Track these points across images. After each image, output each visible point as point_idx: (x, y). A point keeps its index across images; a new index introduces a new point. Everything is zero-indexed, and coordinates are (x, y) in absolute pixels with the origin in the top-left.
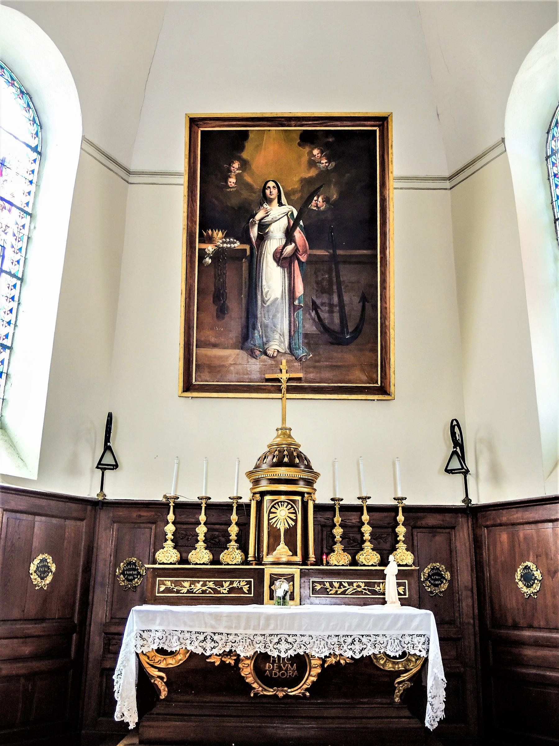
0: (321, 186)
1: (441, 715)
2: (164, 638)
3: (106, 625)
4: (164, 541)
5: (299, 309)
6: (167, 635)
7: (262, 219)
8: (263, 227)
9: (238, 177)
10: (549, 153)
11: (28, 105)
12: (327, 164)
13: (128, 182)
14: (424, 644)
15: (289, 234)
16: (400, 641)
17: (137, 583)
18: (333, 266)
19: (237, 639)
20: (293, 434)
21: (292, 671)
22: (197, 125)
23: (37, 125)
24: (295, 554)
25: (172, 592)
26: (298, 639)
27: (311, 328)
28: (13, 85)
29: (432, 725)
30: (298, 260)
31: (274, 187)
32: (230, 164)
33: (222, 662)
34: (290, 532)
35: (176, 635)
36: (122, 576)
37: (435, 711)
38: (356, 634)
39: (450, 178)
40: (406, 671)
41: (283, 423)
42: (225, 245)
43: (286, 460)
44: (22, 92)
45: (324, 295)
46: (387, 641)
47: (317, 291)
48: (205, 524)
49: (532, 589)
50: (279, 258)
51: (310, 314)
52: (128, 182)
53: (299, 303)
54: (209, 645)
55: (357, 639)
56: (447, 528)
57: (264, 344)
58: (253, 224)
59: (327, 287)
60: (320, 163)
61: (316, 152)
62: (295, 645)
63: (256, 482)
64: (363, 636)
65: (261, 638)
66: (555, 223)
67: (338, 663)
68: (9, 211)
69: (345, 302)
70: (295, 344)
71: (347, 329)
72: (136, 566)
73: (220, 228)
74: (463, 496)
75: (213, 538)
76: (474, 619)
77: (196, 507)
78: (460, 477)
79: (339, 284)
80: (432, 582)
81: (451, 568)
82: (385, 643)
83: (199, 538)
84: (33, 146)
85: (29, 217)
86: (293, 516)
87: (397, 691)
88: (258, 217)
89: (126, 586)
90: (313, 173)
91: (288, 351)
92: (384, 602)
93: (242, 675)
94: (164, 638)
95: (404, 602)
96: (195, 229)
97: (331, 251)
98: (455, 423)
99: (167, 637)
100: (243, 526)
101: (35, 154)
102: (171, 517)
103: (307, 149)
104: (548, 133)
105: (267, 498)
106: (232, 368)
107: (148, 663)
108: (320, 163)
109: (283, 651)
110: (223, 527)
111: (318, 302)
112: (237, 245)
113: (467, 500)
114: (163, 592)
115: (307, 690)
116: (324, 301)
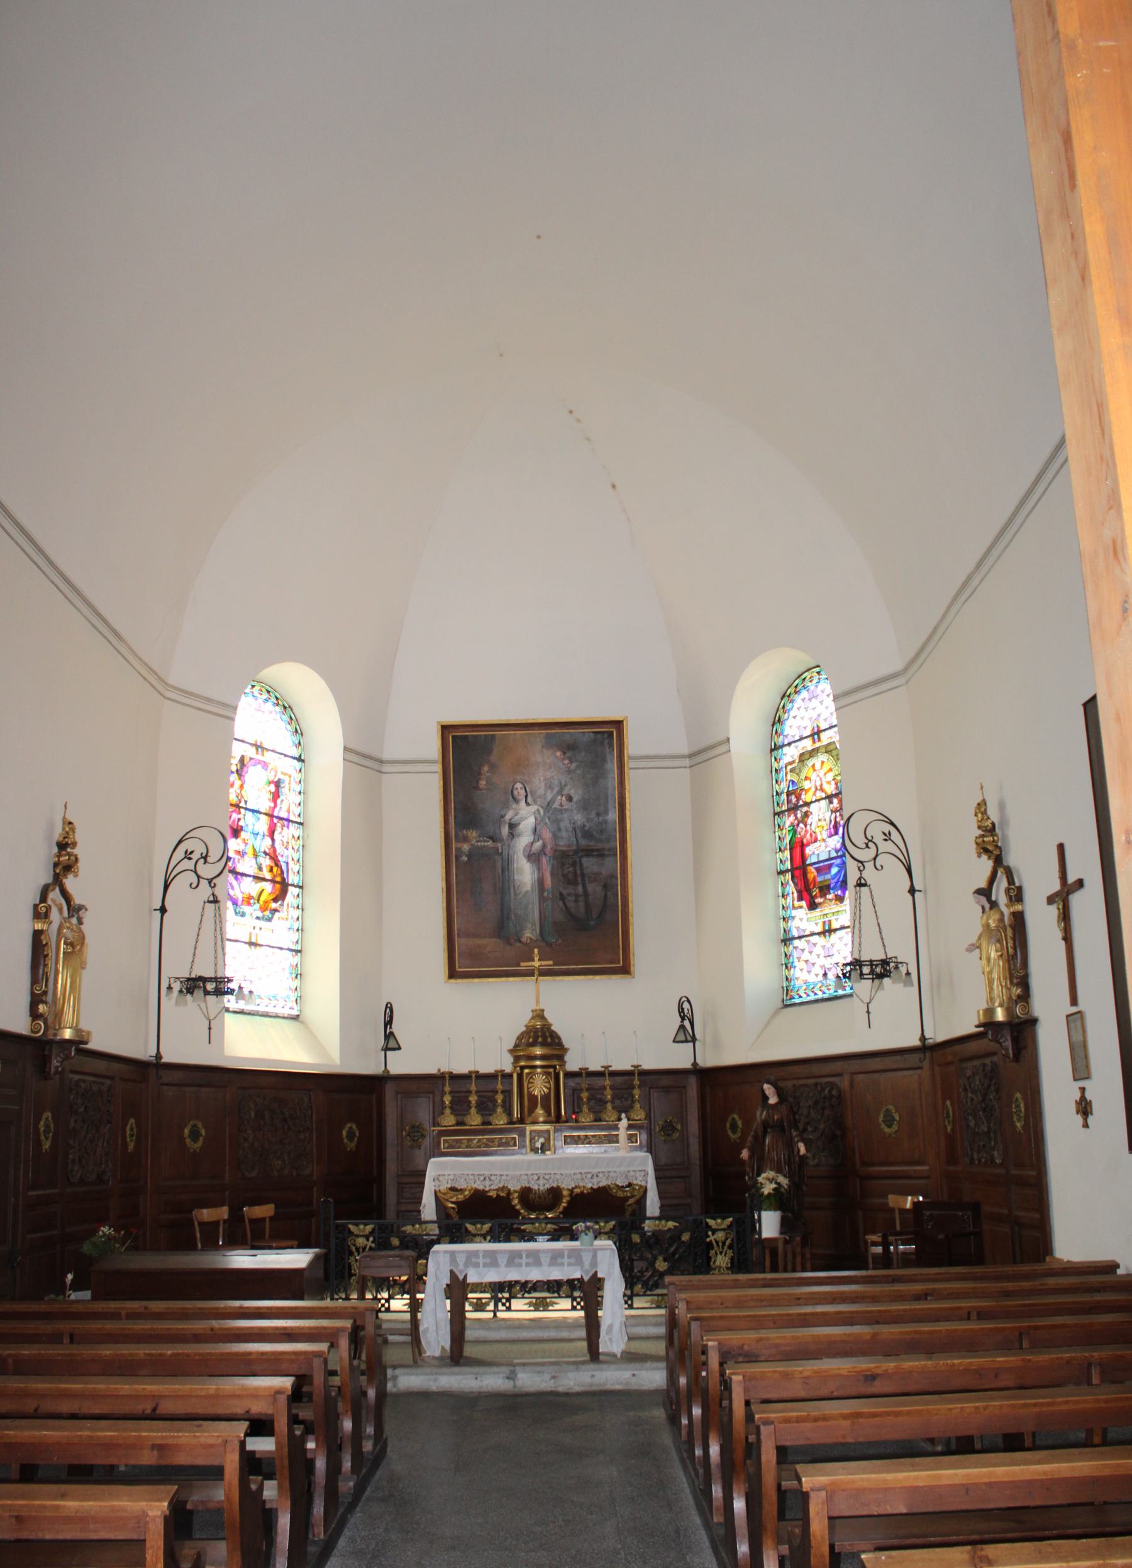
8: (512, 826)
20: (546, 1014)
24: (549, 1114)
27: (560, 917)
28: (277, 704)
33: (498, 1195)
34: (546, 1098)
38: (595, 1171)
39: (690, 756)
40: (632, 1196)
43: (540, 1040)
44: (285, 708)
54: (487, 1183)
63: (517, 1059)
67: (582, 1192)
77: (466, 1077)
84: (297, 756)
88: (508, 817)
100: (508, 1093)
102: (447, 1089)
105: (526, 1071)
110: (490, 1094)
111: (565, 892)
113: (695, 1064)
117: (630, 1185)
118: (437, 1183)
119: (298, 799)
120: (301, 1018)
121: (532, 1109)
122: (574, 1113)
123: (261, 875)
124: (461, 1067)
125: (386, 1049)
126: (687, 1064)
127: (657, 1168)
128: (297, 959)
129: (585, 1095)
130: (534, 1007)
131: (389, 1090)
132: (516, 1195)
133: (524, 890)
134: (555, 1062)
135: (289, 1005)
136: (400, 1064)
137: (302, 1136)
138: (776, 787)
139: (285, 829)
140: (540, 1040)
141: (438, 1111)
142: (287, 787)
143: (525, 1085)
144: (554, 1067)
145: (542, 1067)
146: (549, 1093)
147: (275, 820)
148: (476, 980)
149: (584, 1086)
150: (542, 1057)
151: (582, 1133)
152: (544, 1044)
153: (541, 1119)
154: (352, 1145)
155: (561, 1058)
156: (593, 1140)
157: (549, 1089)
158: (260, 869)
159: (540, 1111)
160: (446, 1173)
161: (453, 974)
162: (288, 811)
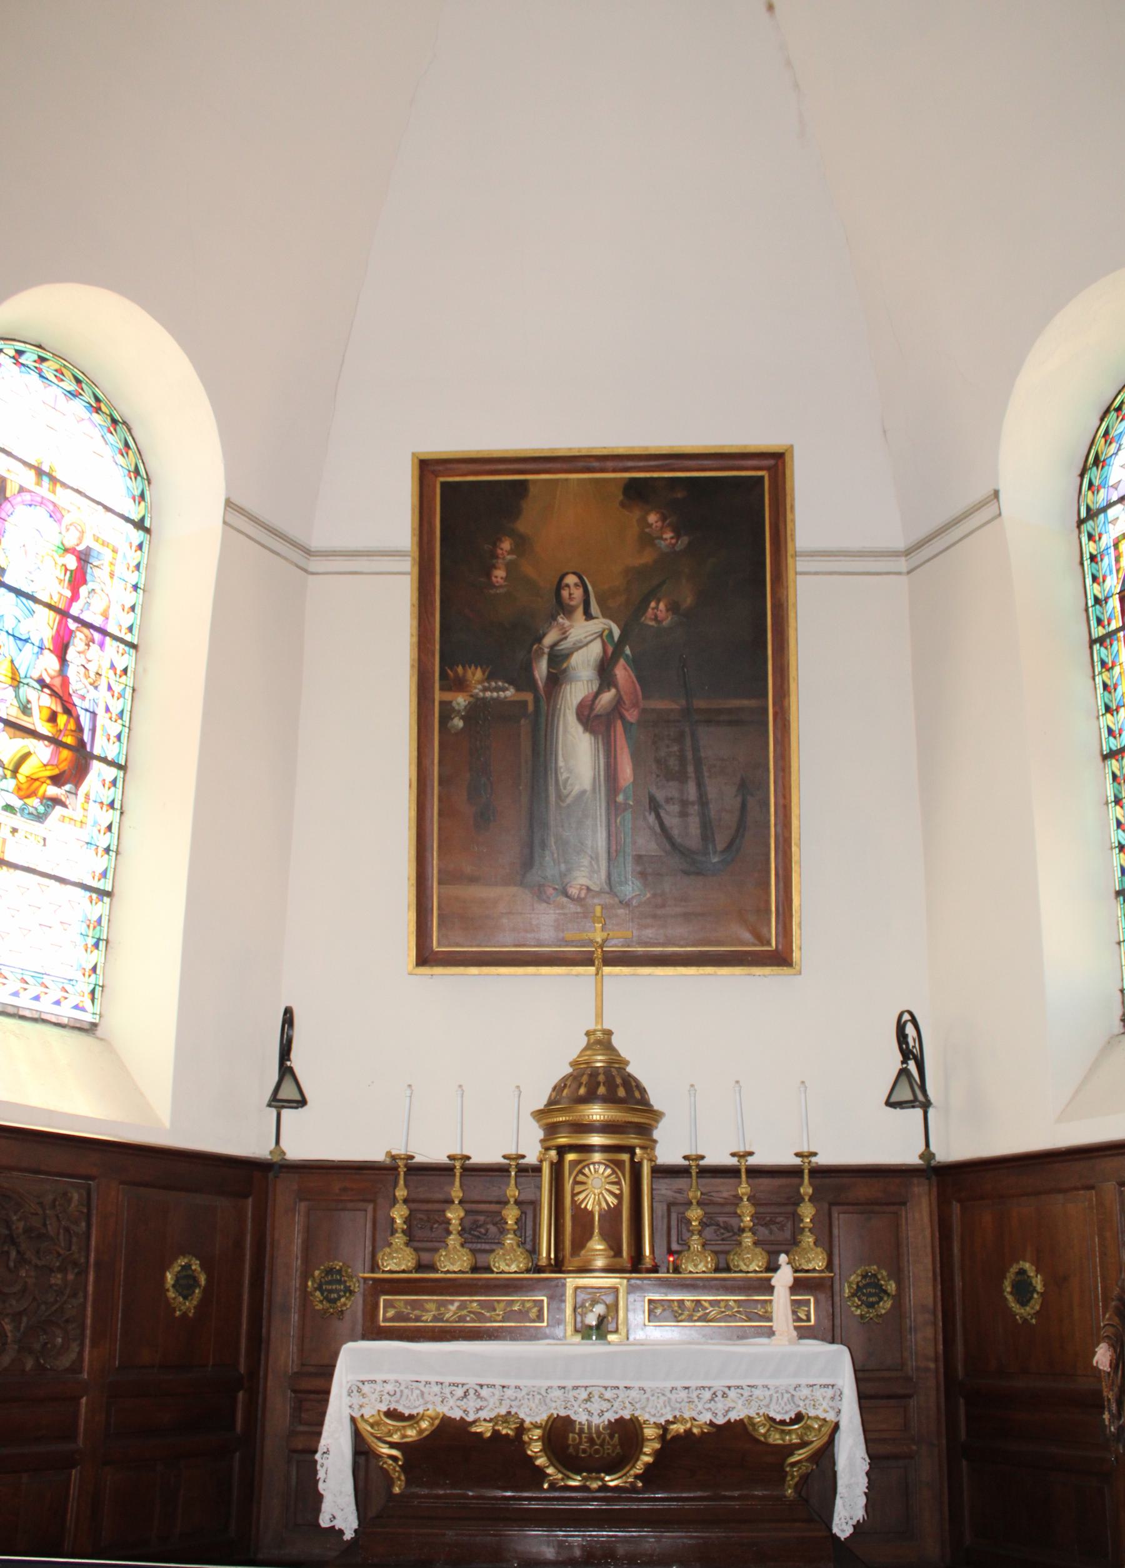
0: (664, 582)
1: (859, 1514)
2: (398, 1394)
3: (297, 1375)
4: (389, 1233)
5: (625, 810)
6: (402, 1388)
7: (556, 644)
8: (558, 659)
9: (510, 567)
10: (1083, 514)
11: (127, 445)
12: (673, 541)
13: (306, 571)
14: (833, 1398)
15: (605, 671)
16: (793, 1396)
17: (345, 1304)
18: (687, 729)
19: (520, 1395)
20: (616, 1041)
21: (612, 1448)
22: (433, 472)
23: (142, 478)
24: (618, 1253)
25: (406, 1319)
26: (622, 1394)
27: (648, 844)
28: (98, 410)
29: (843, 1531)
30: (622, 717)
31: (576, 585)
32: (495, 544)
33: (496, 1433)
34: (612, 1216)
35: (417, 1388)
36: (318, 1293)
37: (849, 1510)
38: (719, 1384)
39: (908, 553)
40: (804, 1444)
41: (597, 1023)
42: (488, 694)
43: (602, 1090)
44: (114, 422)
45: (671, 783)
46: (771, 1396)
47: (658, 776)
48: (461, 1202)
49: (1028, 1308)
50: (587, 716)
51: (645, 818)
52: (306, 571)
53: (626, 799)
55: (719, 1394)
56: (894, 1204)
57: (563, 875)
58: (540, 653)
59: (677, 768)
60: (661, 538)
61: (652, 518)
62: (616, 1404)
63: (551, 1130)
64: (729, 1388)
65: (559, 1393)
66: (1091, 648)
67: (688, 1432)
68: (102, 645)
69: (710, 797)
70: (619, 875)
71: (714, 846)
72: (342, 1276)
73: (477, 662)
74: (922, 1148)
75: (476, 1225)
76: (936, 1360)
77: (442, 1171)
78: (919, 1112)
79: (698, 762)
80: (864, 1298)
81: (898, 1274)
82: (768, 1399)
83: (451, 1228)
85: (132, 651)
86: (615, 1189)
87: (789, 1478)
88: (548, 640)
89: (325, 1311)
90: (647, 557)
91: (607, 888)
92: (770, 1333)
93: (529, 1452)
94: (398, 1394)
95: (804, 1333)
96: (433, 665)
97: (683, 702)
98: (906, 1017)
99: (402, 1391)
101: (141, 533)
102: (401, 1193)
103: (637, 514)
104: (1082, 476)
105: (571, 1157)
106: (504, 921)
107: (372, 1434)
108: (661, 538)
109: (596, 1414)
110: (494, 1207)
111: (660, 796)
112: (510, 693)
113: (927, 1155)
114: (392, 1320)
115: (637, 1477)
116: (670, 795)
117: (799, 1418)
118: (357, 1400)
119: (132, 598)
120: (100, 1032)
121: (580, 1243)
122: (671, 1252)
123: (25, 721)
124: (432, 1150)
125: (277, 1102)
126: (909, 1155)
127: (861, 1375)
128: (101, 908)
129: (695, 1214)
130: (592, 1026)
131: (283, 1193)
132: (537, 1433)
133: (576, 789)
134: (632, 1140)
135: (74, 1000)
136: (308, 1139)
137: (57, 1279)
138: (1095, 590)
139: (95, 647)
140: (602, 1090)
141: (381, 1231)
142: (107, 569)
143: (568, 1186)
144: (631, 1150)
145: (605, 1149)
146: (618, 1209)
147: (72, 625)
148: (474, 970)
149: (694, 1194)
150: (607, 1128)
151: (688, 1297)
152: (610, 1099)
153: (600, 1263)
154: (187, 1306)
155: (644, 1131)
156: (713, 1312)
157: (619, 1197)
158: (25, 709)
159: (597, 1245)
160: (379, 1377)
161: (425, 957)
162: (106, 615)
